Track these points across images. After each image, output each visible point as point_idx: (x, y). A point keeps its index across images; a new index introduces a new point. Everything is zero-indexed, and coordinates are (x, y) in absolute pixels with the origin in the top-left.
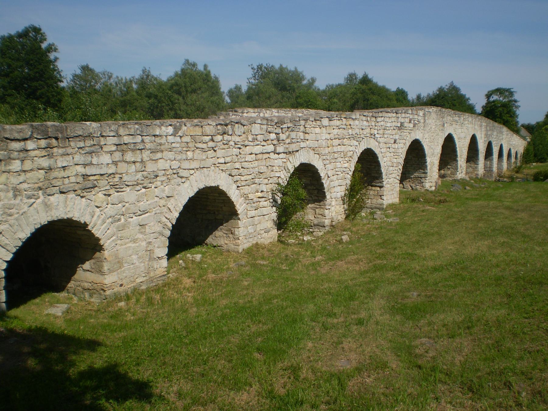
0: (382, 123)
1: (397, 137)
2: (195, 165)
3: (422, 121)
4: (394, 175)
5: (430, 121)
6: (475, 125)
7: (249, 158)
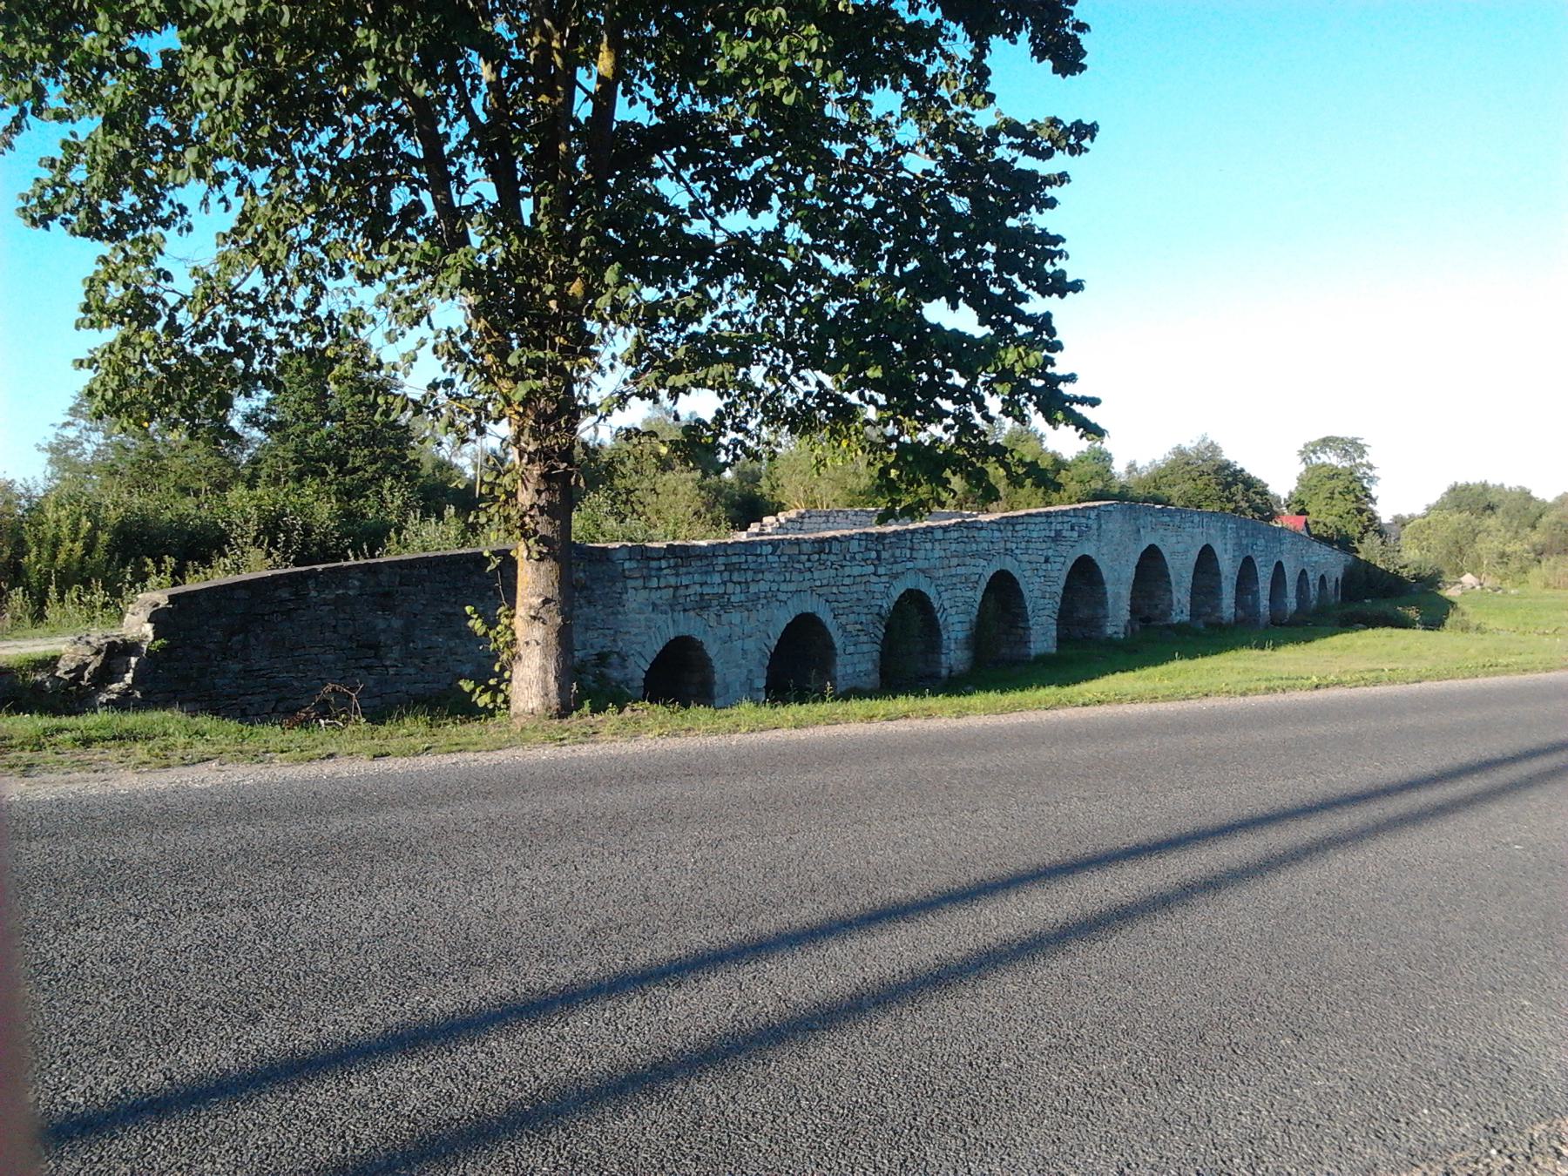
0: (1024, 533)
1: (1050, 552)
2: (792, 587)
3: (1095, 526)
4: (1046, 612)
5: (1111, 526)
6: (1208, 529)
7: (847, 581)
